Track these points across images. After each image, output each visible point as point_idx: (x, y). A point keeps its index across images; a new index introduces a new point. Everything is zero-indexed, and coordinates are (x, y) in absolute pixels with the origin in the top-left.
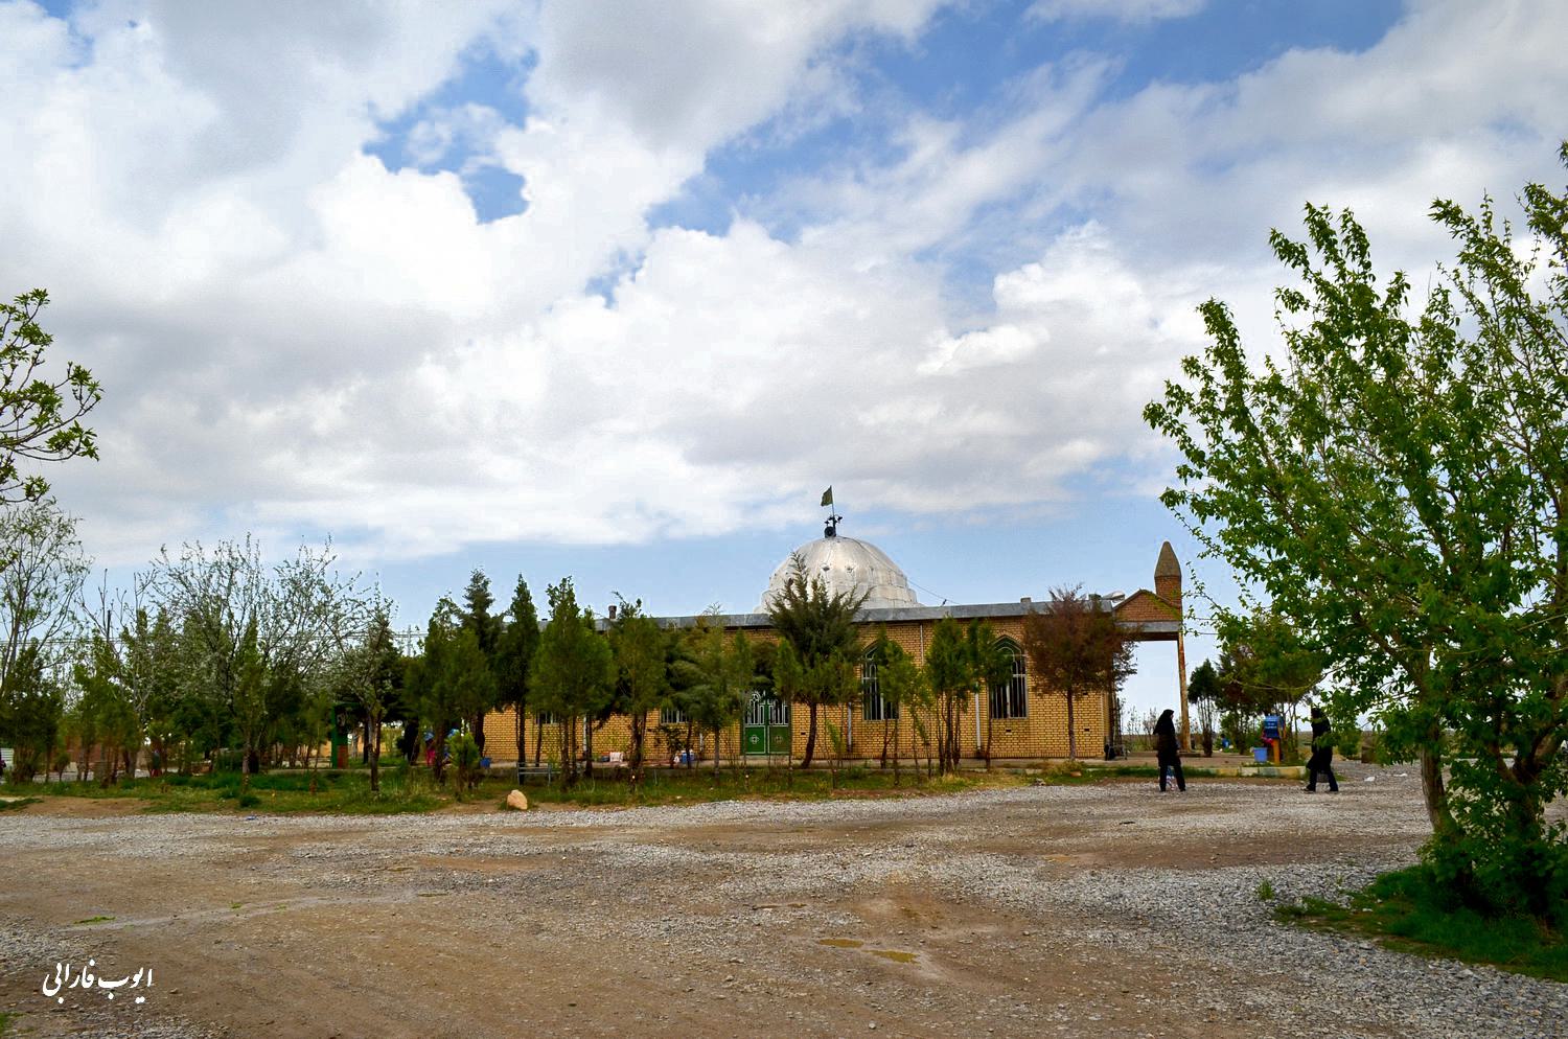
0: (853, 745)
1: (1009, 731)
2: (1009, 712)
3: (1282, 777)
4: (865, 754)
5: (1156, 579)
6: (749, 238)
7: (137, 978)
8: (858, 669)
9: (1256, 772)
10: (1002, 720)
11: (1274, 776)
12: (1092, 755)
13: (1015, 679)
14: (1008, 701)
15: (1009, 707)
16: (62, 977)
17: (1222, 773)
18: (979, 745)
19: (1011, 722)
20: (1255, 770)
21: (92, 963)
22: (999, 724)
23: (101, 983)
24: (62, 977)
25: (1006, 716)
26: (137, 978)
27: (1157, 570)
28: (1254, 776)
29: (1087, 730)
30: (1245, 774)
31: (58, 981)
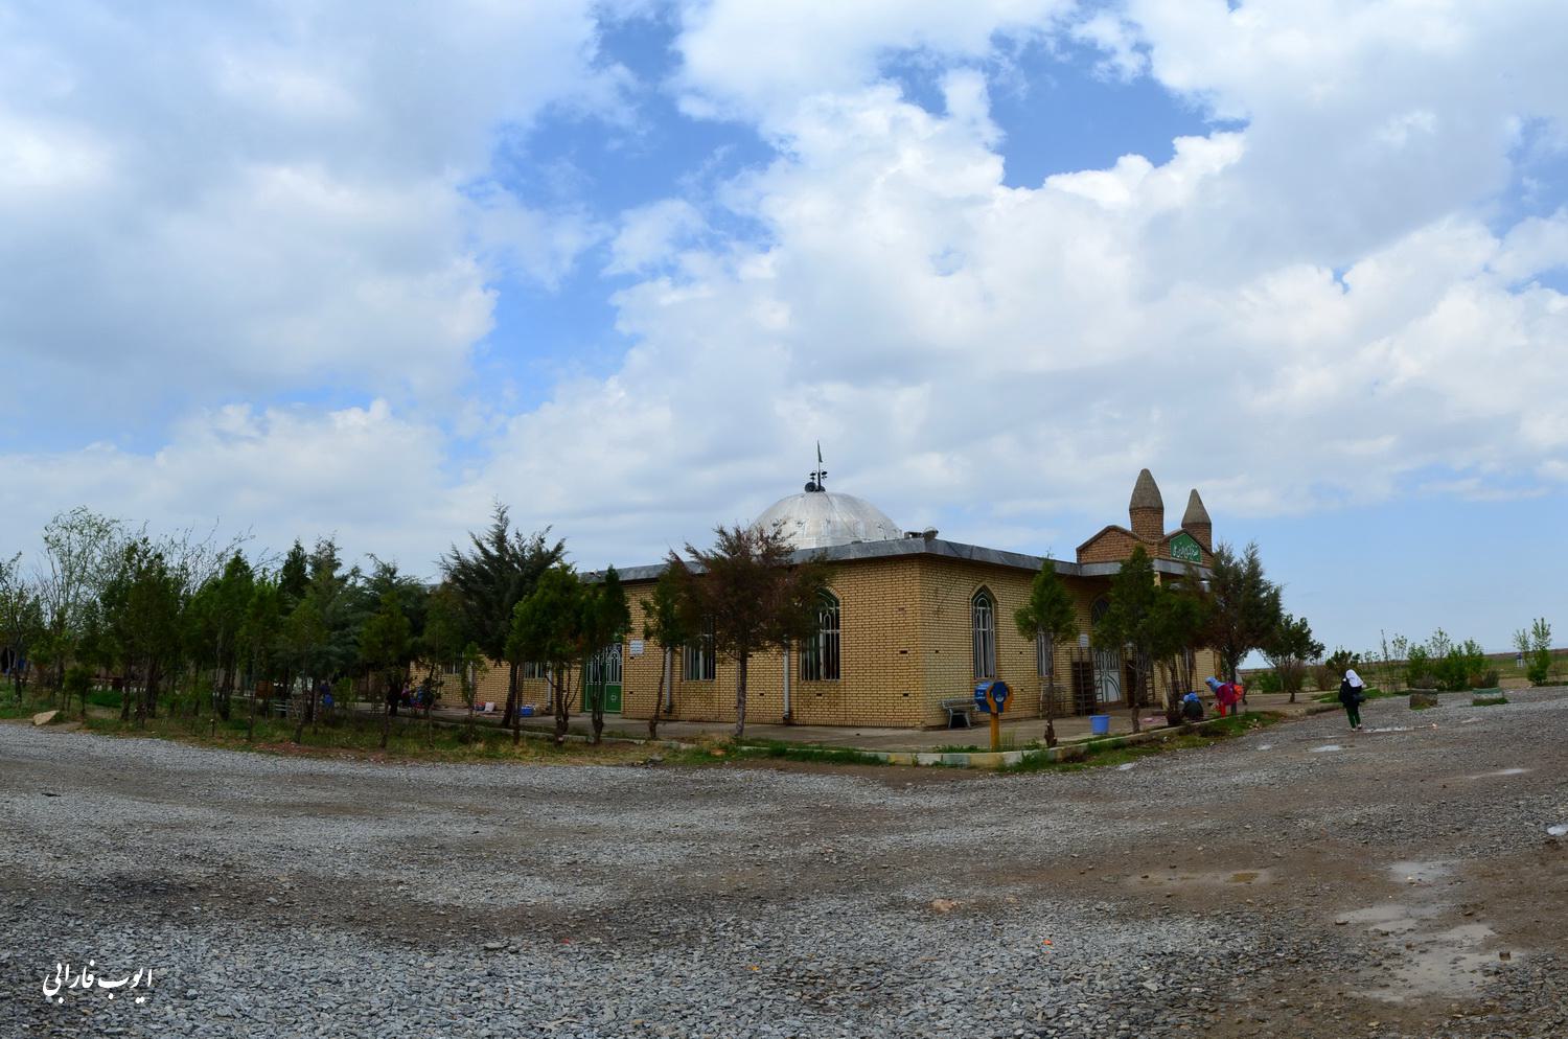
0: (671, 706)
1: (820, 695)
2: (822, 673)
3: (972, 767)
4: (682, 716)
5: (1132, 511)
6: (1174, 75)
7: (137, 978)
8: (747, 612)
9: (939, 760)
10: (813, 682)
11: (962, 766)
12: (910, 724)
13: (828, 635)
14: (822, 660)
15: (822, 667)
16: (62, 977)
17: (893, 760)
18: (786, 709)
19: (825, 685)
20: (936, 757)
21: (92, 963)
22: (811, 687)
23: (102, 983)
24: (62, 977)
25: (818, 678)
26: (137, 978)
27: (1132, 503)
28: (936, 764)
29: (906, 695)
30: (924, 763)
31: (58, 981)
